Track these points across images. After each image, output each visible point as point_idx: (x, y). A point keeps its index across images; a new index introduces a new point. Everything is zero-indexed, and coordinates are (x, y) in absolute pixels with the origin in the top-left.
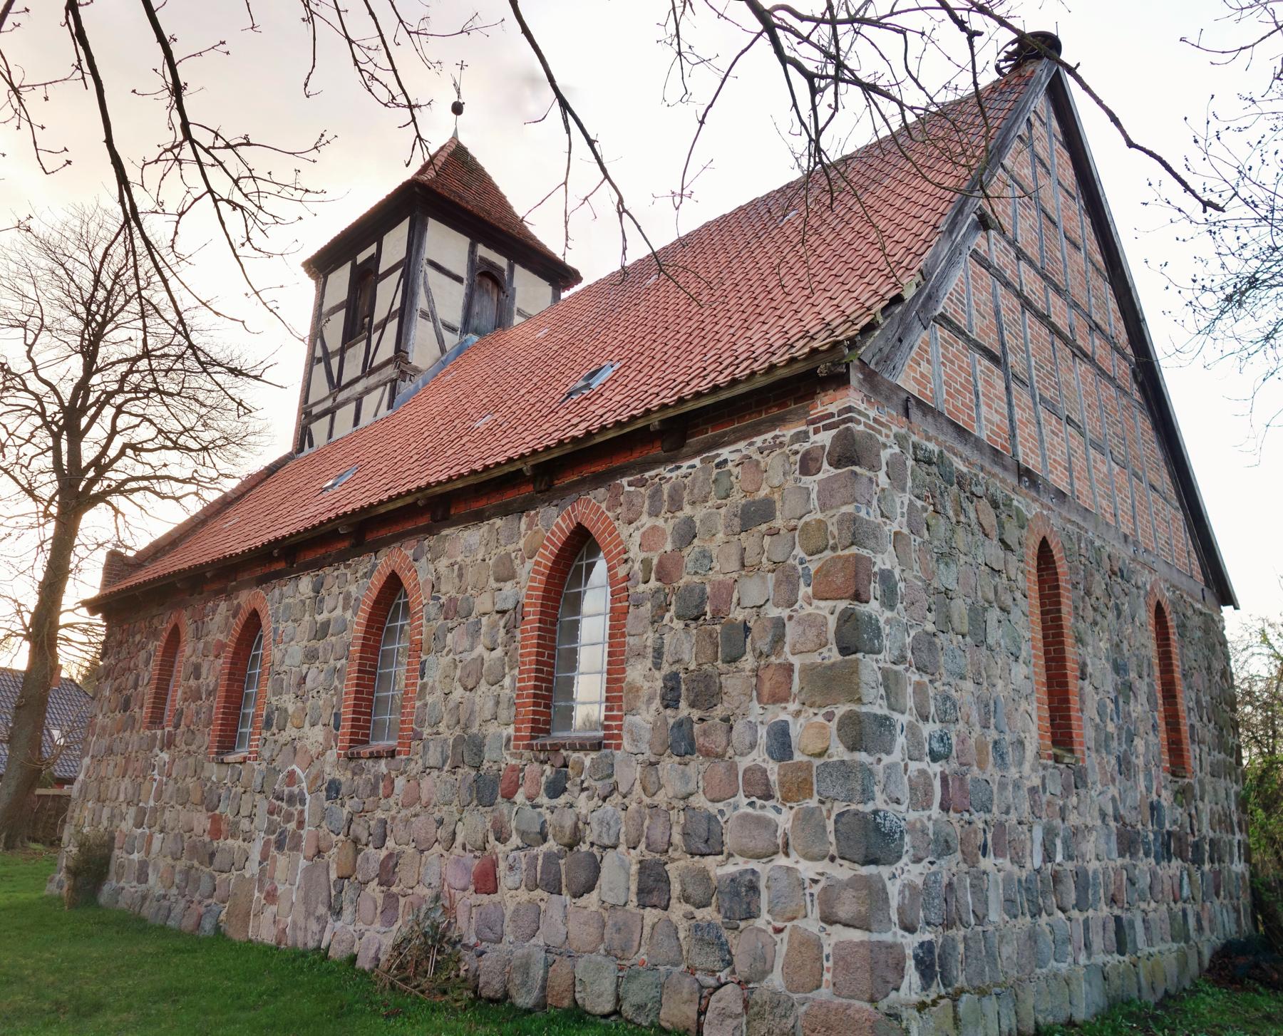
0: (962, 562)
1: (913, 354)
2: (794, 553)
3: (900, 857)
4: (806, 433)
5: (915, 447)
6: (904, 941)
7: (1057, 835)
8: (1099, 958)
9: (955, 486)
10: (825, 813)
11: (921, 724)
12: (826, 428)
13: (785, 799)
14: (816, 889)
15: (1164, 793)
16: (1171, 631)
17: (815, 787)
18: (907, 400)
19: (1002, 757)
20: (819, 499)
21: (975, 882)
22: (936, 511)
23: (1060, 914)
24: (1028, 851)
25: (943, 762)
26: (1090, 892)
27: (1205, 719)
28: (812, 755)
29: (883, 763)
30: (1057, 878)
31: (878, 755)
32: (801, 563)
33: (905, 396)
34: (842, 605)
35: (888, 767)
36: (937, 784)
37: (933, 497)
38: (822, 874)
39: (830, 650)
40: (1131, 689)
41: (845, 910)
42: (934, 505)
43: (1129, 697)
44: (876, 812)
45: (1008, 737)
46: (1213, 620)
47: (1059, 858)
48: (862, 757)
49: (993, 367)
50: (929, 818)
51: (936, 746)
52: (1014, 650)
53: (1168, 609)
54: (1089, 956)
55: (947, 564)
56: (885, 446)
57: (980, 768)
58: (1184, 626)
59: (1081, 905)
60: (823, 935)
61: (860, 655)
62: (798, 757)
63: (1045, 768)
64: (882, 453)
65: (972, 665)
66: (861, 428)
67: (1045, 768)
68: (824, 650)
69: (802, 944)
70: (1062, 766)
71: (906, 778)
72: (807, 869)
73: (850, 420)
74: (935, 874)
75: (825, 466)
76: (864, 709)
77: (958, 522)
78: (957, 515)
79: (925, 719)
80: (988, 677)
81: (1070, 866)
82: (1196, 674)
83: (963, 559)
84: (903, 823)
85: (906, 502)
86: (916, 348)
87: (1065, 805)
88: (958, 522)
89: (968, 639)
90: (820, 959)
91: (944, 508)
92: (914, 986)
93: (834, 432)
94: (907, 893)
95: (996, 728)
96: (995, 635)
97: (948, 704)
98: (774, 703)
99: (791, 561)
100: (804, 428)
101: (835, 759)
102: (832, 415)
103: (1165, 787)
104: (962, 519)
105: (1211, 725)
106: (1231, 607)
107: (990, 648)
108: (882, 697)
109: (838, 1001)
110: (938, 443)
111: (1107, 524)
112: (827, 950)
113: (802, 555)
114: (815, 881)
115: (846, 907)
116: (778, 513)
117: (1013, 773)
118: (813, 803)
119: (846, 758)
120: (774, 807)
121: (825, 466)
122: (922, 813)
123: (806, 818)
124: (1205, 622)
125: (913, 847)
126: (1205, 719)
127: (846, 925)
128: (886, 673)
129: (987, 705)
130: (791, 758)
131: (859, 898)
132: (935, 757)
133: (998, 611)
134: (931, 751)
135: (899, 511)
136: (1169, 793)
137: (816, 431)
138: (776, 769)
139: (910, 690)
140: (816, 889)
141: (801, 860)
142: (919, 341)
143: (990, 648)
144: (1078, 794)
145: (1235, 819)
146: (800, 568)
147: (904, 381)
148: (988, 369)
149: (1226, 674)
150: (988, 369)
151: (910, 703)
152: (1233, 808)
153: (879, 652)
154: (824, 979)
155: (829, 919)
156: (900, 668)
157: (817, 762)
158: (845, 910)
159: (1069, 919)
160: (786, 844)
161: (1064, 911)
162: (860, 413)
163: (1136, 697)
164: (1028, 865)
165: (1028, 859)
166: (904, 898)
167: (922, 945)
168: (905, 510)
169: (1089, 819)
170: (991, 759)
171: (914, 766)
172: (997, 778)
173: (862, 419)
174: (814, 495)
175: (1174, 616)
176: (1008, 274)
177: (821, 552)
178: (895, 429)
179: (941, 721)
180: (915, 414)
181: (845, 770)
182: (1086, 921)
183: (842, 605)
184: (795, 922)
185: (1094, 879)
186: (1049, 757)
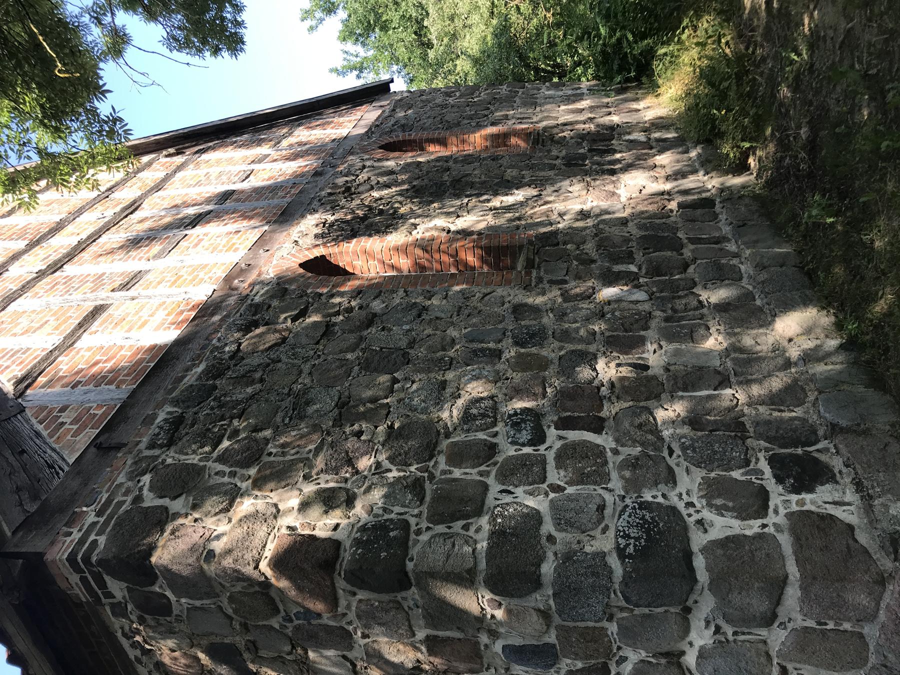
0: (307, 381)
2: (277, 626)
3: (674, 510)
4: (113, 606)
5: (152, 446)
6: (782, 511)
7: (609, 270)
8: (726, 230)
9: (218, 382)
10: (625, 615)
11: (500, 458)
12: (103, 585)
13: (609, 655)
14: (729, 630)
15: (555, 153)
16: (407, 138)
17: (591, 624)
19: (532, 336)
20: (201, 599)
21: (680, 385)
23: (691, 269)
24: (632, 306)
25: (544, 422)
26: (661, 234)
27: (486, 112)
28: (548, 626)
29: (554, 533)
30: (655, 270)
31: (544, 540)
32: (291, 621)
33: (93, 450)
34: (341, 584)
35: (558, 524)
36: (574, 435)
37: (222, 418)
38: (708, 623)
39: (405, 599)
40: (459, 180)
41: (759, 604)
43: (467, 183)
44: (621, 552)
45: (510, 324)
46: (400, 100)
47: (633, 268)
48: (548, 568)
50: (616, 452)
51: (525, 436)
52: (414, 312)
53: (387, 139)
54: (725, 239)
55: (308, 403)
56: (138, 499)
58: (403, 126)
59: (678, 246)
60: (790, 626)
61: (410, 565)
62: (552, 638)
63: (540, 280)
64: (146, 504)
65: (429, 371)
66: (102, 540)
67: (540, 280)
69: (803, 650)
71: (570, 490)
72: (700, 637)
74: (684, 448)
77: (262, 380)
78: (252, 382)
79: (492, 449)
80: (444, 349)
81: (639, 256)
82: (446, 118)
84: (628, 501)
85: (220, 467)
86: (40, 428)
87: (577, 258)
88: (262, 380)
90: (824, 632)
91: (238, 402)
92: (837, 497)
93: (107, 578)
94: (719, 502)
95: (500, 341)
96: (398, 335)
97: (474, 411)
98: (481, 658)
99: (289, 631)
101: (551, 602)
102: (84, 580)
103: (549, 151)
104: (258, 375)
105: (492, 108)
106: (391, 85)
107: (412, 344)
109: (882, 615)
111: (301, 192)
112: (811, 623)
114: (718, 629)
115: (754, 601)
116: (226, 641)
118: (613, 628)
119: (550, 592)
120: (618, 663)
122: (611, 465)
123: (629, 634)
124: (402, 107)
125: (656, 484)
126: (486, 112)
127: (778, 602)
128: (436, 518)
129: (475, 352)
130: (553, 646)
131: (742, 588)
132: (539, 438)
133: (373, 330)
134: (531, 443)
135: (226, 479)
136: (553, 148)
137: (110, 595)
138: (569, 661)
139: (457, 473)
140: (729, 630)
141: (688, 639)
142: (34, 421)
143: (412, 344)
144: (565, 243)
145: (570, 92)
146: (296, 622)
147: (73, 451)
148: (101, 325)
150: (101, 325)
151: (472, 474)
152: (561, 93)
153: (406, 525)
154: (850, 629)
155: (769, 620)
156: (429, 487)
157: (557, 620)
158: (759, 604)
159: (694, 260)
160: (667, 655)
161: (686, 266)
162: (82, 541)
163: (467, 175)
164: (647, 307)
165: (640, 307)
166: (727, 509)
167: (780, 480)
168: (227, 470)
170: (534, 350)
172: (557, 344)
173: (92, 537)
174: (198, 603)
175: (393, 135)
178: (121, 479)
180: (120, 435)
181: (566, 591)
182: (692, 241)
183: (341, 584)
184: (773, 654)
185: (647, 229)
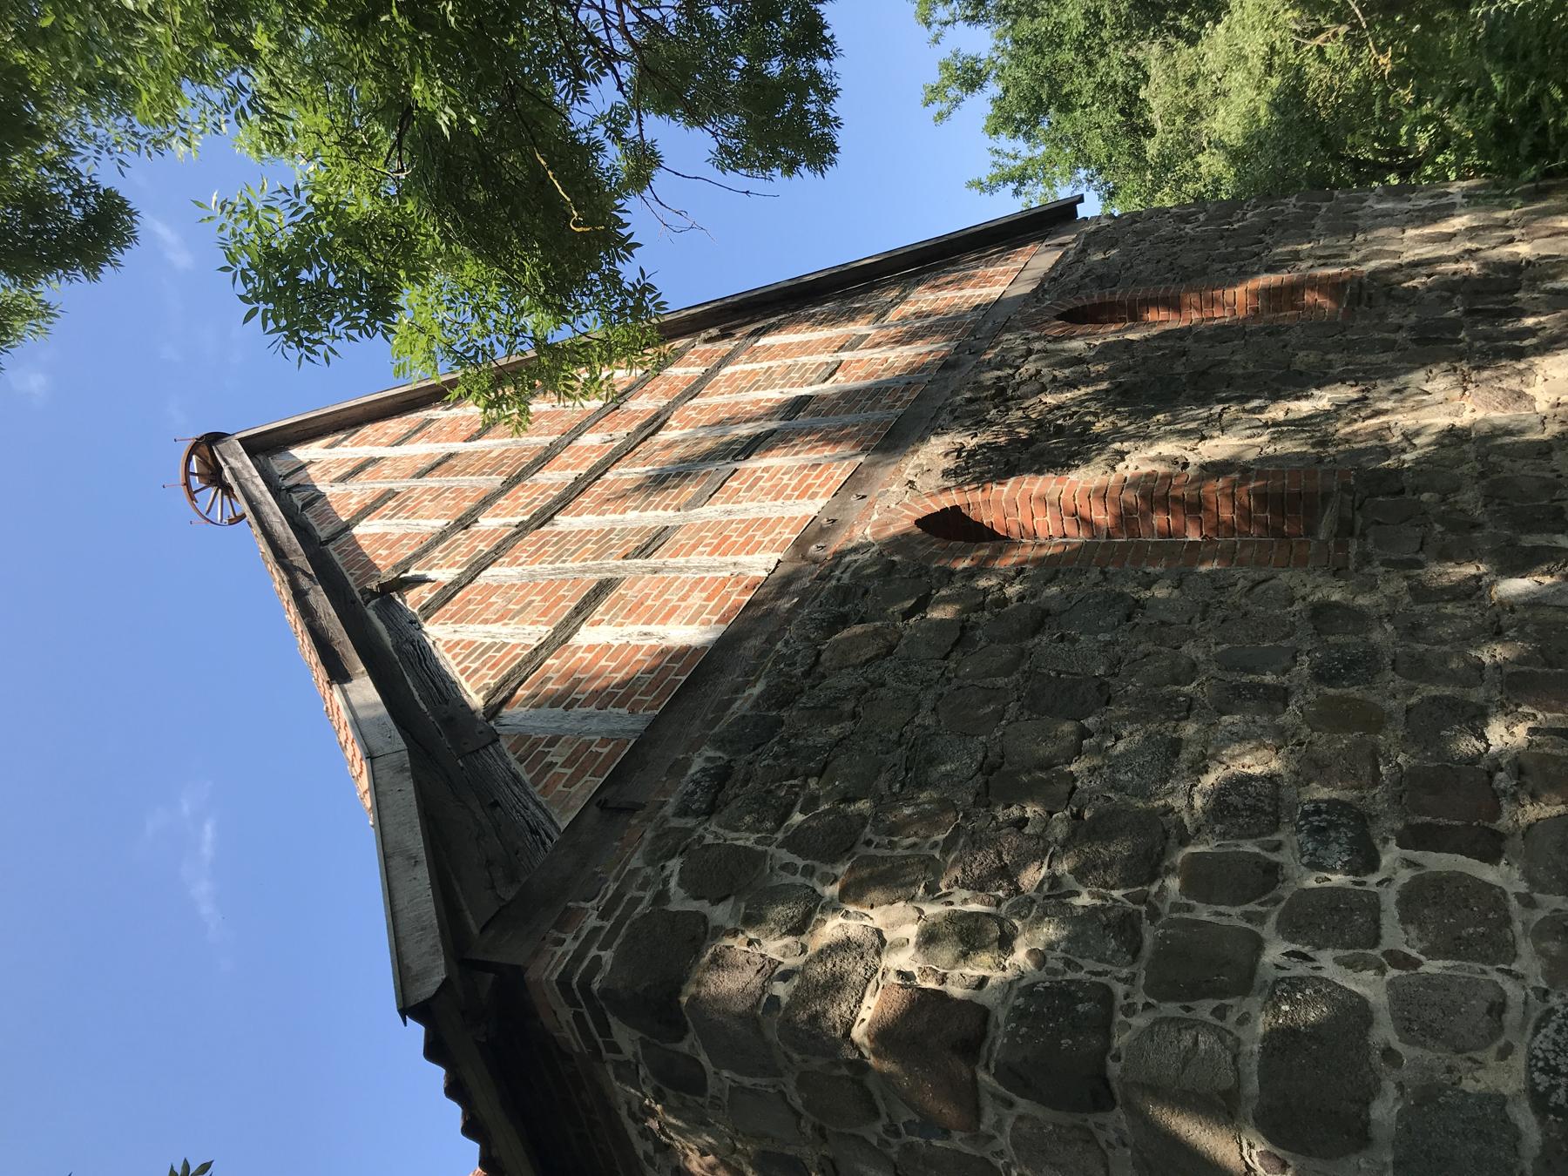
1: (526, 778)
4: (618, 1065)
5: (683, 812)
12: (605, 1029)
15: (1393, 318)
18: (603, 806)
22: (820, 774)
25: (1376, 832)
27: (1255, 248)
32: (897, 1134)
33: (594, 810)
35: (1405, 1029)
39: (1102, 1126)
40: (1204, 373)
42: (807, 776)
46: (1096, 232)
48: (1384, 1111)
49: (614, 595)
56: (662, 897)
57: (1378, 726)
63: (1365, 559)
64: (674, 907)
68: (1102, 1137)
70: (1359, 521)
73: (585, 985)
75: (684, 1047)
76: (1253, 1086)
77: (854, 716)
78: (839, 719)
82: (1181, 261)
83: (925, 719)
85: (786, 856)
86: (520, 769)
88: (854, 716)
89: (1090, 722)
93: (612, 1020)
100: (610, 1068)
102: (578, 1017)
103: (1382, 316)
104: (848, 707)
108: (1220, 1012)
110: (695, 746)
113: (879, 1126)
117: (1383, 636)
121: (684, 1047)
122: (1518, 927)
126: (1255, 248)
139: (1204, 913)
142: (511, 757)
148: (607, 612)
149: (1259, 956)
151: (1233, 916)
152: (1407, 206)
153: (1106, 995)
156: (1150, 935)
168: (800, 863)
169: (1465, 468)
171: (1394, 935)
174: (748, 1082)
175: (1083, 294)
176: (484, 547)
177: (869, 1095)
179: (1275, 826)
186: (1342, 546)
